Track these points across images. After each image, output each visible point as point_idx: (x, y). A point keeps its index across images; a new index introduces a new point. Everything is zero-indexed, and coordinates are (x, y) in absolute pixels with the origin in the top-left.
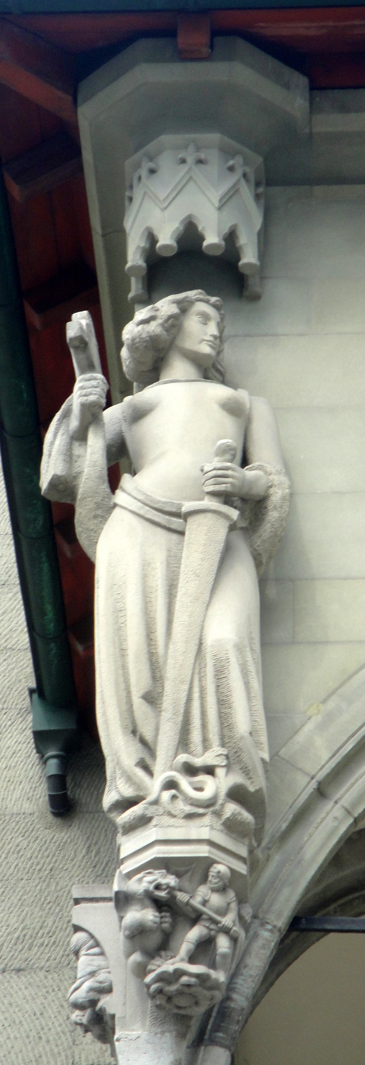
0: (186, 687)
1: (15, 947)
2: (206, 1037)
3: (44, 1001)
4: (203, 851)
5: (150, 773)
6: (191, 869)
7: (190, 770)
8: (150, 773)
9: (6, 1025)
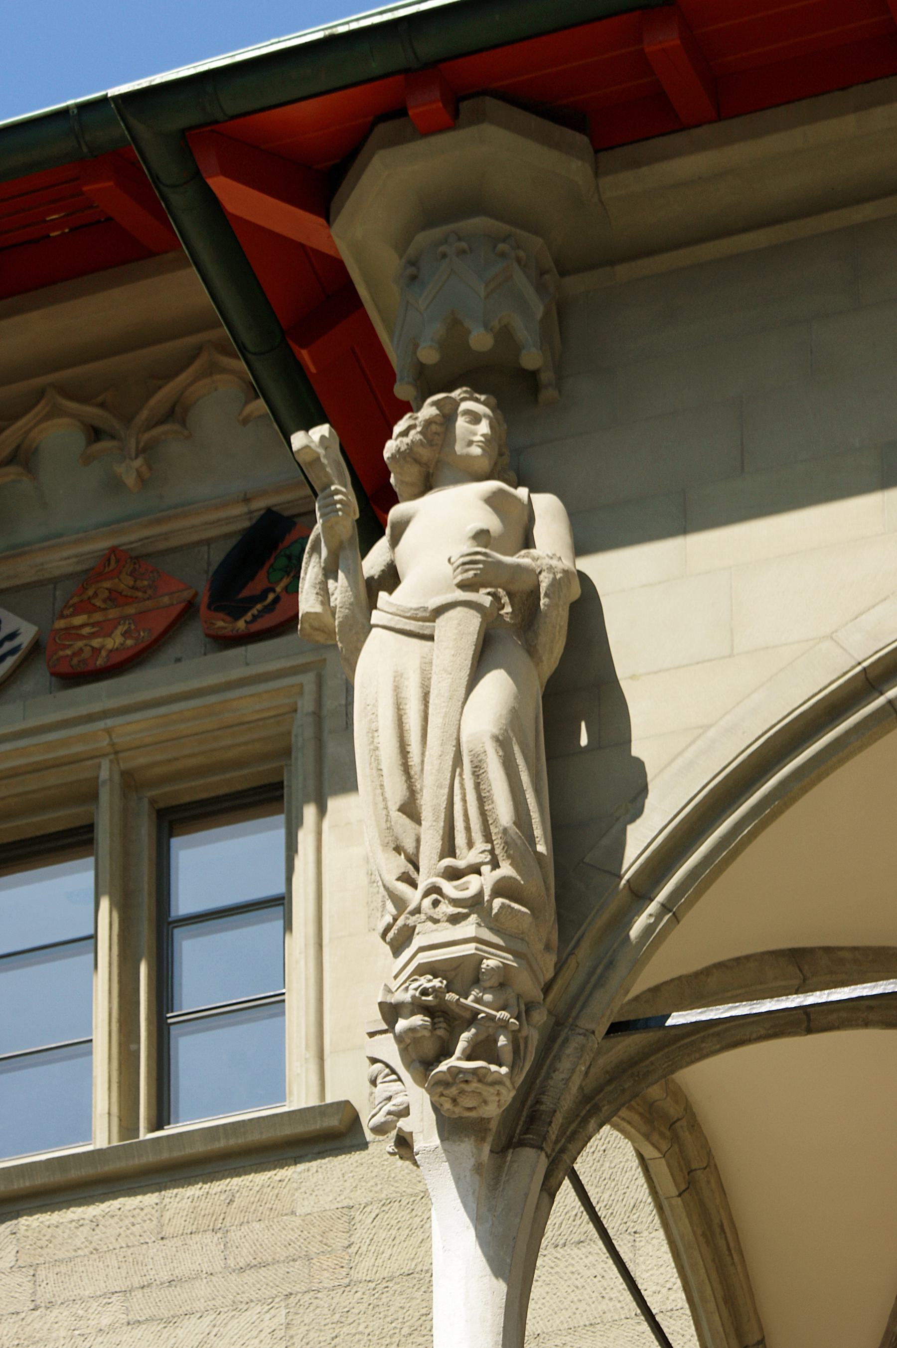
0: (446, 791)
1: (574, 1223)
2: (515, 1140)
3: (604, 1266)
4: (469, 949)
5: (414, 884)
6: (460, 974)
7: (454, 874)
8: (414, 884)
9: (570, 1291)
